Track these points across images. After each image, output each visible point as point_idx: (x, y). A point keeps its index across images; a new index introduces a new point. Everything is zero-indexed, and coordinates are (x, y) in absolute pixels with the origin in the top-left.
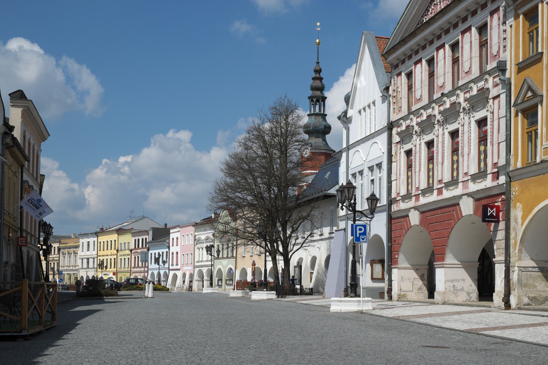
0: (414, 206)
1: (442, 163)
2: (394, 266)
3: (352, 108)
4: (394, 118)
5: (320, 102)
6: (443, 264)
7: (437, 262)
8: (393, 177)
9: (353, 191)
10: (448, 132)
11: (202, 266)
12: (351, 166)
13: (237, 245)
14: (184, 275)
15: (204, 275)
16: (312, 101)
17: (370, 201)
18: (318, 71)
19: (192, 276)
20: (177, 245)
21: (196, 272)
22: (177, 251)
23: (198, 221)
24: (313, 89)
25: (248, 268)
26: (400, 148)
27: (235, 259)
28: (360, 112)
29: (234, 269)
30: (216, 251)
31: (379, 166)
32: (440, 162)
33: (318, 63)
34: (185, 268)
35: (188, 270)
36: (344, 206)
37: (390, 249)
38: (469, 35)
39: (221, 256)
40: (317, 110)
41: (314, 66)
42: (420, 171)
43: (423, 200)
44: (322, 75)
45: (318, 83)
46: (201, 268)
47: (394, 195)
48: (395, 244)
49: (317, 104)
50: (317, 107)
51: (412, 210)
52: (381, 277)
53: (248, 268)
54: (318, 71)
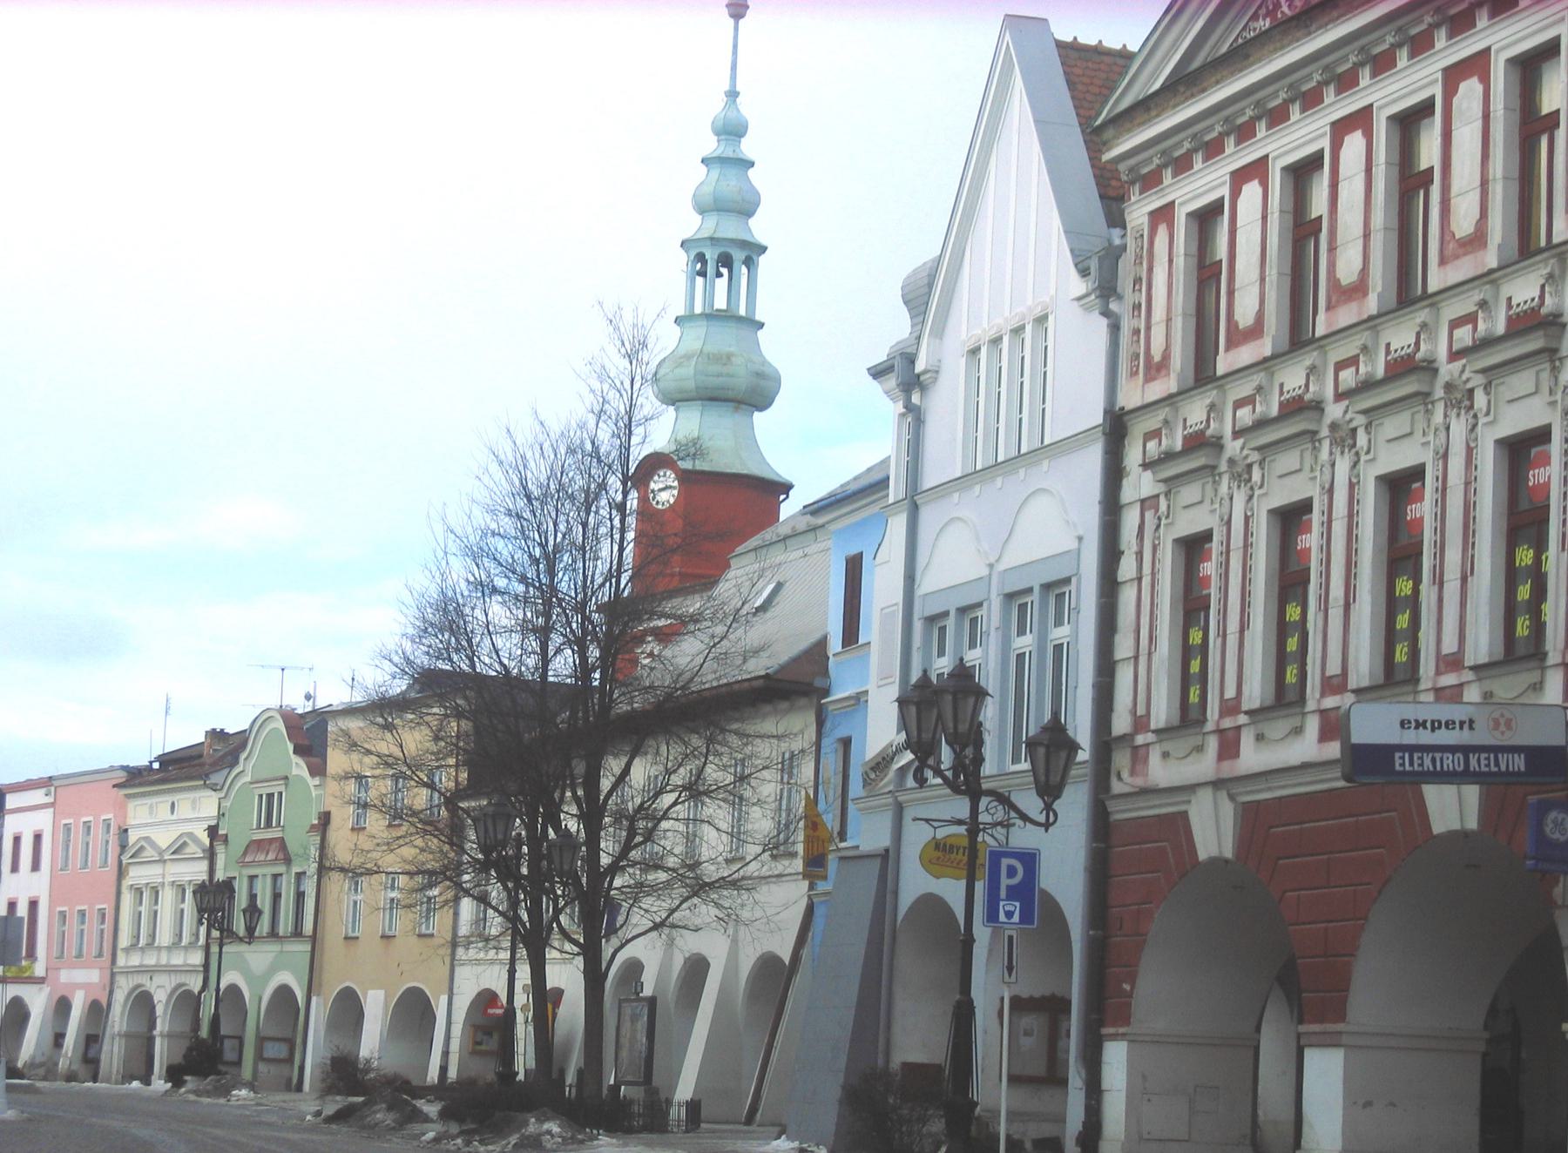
0: (1213, 779)
1: (1347, 607)
2: (1112, 1030)
3: (939, 332)
4: (1131, 396)
5: (736, 265)
6: (1340, 1033)
7: (1310, 1022)
8: (1123, 647)
9: (976, 711)
10: (1376, 477)
11: (151, 971)
12: (928, 583)
13: (435, 909)
14: (62, 1007)
15: (159, 1010)
16: (701, 258)
17: (913, 709)
18: (731, 130)
19: (97, 1011)
20: (36, 866)
21: (120, 997)
22: (33, 894)
23: (140, 759)
24: (707, 206)
25: (371, 993)
26: (1158, 526)
27: (309, 948)
28: (974, 352)
29: (300, 996)
30: (244, 911)
31: (1056, 589)
32: (1336, 599)
33: (733, 94)
34: (65, 976)
35: (82, 981)
36: (930, 767)
37: (1099, 953)
38: (1479, 88)
39: (264, 926)
40: (720, 303)
41: (715, 105)
42: (1243, 627)
43: (1252, 758)
44: (748, 147)
45: (730, 185)
46: (143, 980)
47: (1121, 723)
48: (1118, 933)
49: (719, 275)
50: (721, 284)
51: (1206, 795)
52: (624, 1005)
53: (371, 993)
54: (731, 130)
